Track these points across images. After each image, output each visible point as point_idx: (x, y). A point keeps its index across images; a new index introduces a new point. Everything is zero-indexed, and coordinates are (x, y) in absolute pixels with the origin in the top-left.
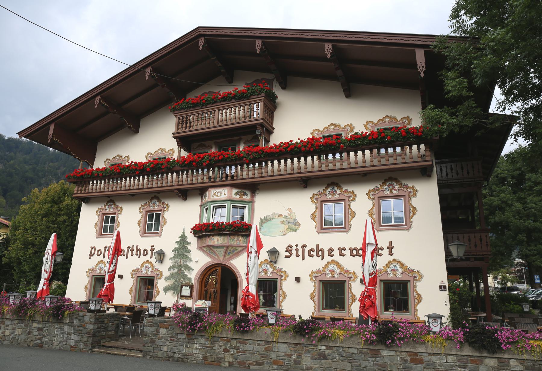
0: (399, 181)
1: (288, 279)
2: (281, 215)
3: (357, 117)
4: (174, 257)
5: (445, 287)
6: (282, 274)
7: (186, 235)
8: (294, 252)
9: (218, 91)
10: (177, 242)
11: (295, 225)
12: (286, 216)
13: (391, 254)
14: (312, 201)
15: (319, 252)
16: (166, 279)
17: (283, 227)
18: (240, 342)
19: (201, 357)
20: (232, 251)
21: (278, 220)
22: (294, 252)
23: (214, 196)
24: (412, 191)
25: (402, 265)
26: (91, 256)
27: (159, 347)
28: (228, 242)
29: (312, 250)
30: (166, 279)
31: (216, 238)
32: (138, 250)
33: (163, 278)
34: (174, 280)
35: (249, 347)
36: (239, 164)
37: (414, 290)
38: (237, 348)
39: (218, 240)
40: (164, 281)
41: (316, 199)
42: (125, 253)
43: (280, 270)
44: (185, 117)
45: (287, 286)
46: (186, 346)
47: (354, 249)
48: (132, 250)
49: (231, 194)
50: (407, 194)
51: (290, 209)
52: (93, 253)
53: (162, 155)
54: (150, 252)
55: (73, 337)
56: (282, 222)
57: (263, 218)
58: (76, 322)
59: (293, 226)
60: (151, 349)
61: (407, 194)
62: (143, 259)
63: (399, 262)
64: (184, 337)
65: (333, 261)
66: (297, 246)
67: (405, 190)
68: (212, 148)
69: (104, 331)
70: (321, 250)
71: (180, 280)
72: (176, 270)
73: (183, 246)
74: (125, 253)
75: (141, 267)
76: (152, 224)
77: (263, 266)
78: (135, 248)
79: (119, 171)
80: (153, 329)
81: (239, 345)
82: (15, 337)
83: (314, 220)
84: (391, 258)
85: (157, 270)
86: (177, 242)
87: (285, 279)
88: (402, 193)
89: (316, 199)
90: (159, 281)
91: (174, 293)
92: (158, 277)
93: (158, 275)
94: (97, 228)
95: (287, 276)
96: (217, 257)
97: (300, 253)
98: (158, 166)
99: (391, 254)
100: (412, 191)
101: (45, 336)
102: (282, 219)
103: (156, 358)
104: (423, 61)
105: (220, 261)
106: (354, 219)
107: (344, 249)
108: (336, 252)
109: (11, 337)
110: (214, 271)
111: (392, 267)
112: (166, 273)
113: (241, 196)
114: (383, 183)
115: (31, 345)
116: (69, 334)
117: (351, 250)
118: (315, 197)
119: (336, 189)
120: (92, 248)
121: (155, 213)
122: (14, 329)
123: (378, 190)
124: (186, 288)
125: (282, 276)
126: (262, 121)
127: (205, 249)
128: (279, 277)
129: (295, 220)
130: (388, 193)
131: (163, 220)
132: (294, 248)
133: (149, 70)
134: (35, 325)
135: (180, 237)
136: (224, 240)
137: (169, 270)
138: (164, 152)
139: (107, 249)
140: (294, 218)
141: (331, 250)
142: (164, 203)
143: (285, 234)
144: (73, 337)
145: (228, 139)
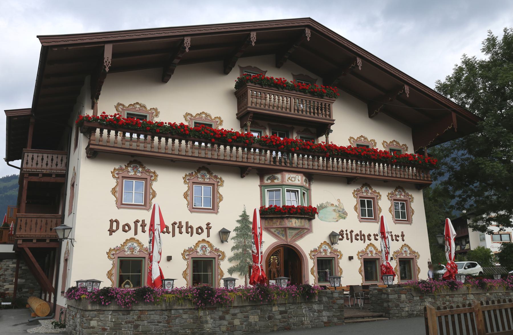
0: (142, 165)
1: (343, 258)
2: (332, 205)
3: (380, 137)
4: (236, 237)
6: (338, 254)
7: (248, 214)
12: (336, 206)
14: (354, 196)
15: (361, 237)
16: (230, 260)
17: (335, 215)
18: (451, 297)
20: (302, 232)
22: (345, 236)
24: (153, 175)
25: (409, 248)
26: (111, 231)
27: (402, 309)
29: (357, 235)
30: (230, 260)
31: (294, 221)
33: (226, 259)
34: (239, 261)
35: (455, 299)
36: (316, 155)
37: (219, 267)
38: (449, 301)
39: (295, 223)
40: (228, 262)
41: (357, 194)
42: (171, 230)
43: (336, 251)
44: (323, 104)
45: (343, 263)
46: (420, 305)
50: (149, 178)
51: (339, 200)
52: (114, 228)
54: (205, 231)
55: (324, 313)
56: (334, 210)
57: (319, 205)
58: (325, 299)
59: (343, 215)
60: (397, 311)
61: (149, 178)
62: (197, 238)
63: (408, 246)
64: (418, 298)
66: (346, 231)
67: (148, 174)
68: (265, 129)
71: (246, 260)
72: (240, 250)
73: (246, 225)
74: (171, 230)
75: (195, 247)
77: (323, 247)
78: (184, 224)
79: (137, 123)
81: (450, 299)
82: (250, 324)
84: (403, 243)
85: (217, 250)
87: (341, 258)
88: (144, 176)
89: (357, 194)
90: (222, 263)
91: (241, 274)
92: (220, 258)
93: (219, 255)
95: (342, 255)
96: (284, 238)
97: (349, 237)
98: (203, 132)
99: (403, 240)
100: (153, 175)
101: (291, 317)
102: (334, 208)
103: (402, 317)
104: (456, 122)
105: (287, 242)
108: (372, 237)
109: (244, 326)
110: (278, 251)
111: (404, 249)
112: (229, 254)
113: (272, 181)
114: (128, 164)
115: (275, 329)
116: (319, 311)
118: (356, 193)
119: (368, 189)
120: (111, 221)
122: (247, 317)
123: (393, 194)
125: (338, 255)
127: (273, 230)
128: (336, 256)
129: (343, 209)
130: (132, 173)
131: (218, 195)
132: (345, 232)
134: (275, 309)
135: (241, 216)
136: (301, 223)
137: (232, 250)
138: (209, 118)
139: (176, 226)
140: (342, 207)
141: (369, 235)
142: (216, 177)
143: (337, 221)
144: (324, 313)
145: (281, 124)
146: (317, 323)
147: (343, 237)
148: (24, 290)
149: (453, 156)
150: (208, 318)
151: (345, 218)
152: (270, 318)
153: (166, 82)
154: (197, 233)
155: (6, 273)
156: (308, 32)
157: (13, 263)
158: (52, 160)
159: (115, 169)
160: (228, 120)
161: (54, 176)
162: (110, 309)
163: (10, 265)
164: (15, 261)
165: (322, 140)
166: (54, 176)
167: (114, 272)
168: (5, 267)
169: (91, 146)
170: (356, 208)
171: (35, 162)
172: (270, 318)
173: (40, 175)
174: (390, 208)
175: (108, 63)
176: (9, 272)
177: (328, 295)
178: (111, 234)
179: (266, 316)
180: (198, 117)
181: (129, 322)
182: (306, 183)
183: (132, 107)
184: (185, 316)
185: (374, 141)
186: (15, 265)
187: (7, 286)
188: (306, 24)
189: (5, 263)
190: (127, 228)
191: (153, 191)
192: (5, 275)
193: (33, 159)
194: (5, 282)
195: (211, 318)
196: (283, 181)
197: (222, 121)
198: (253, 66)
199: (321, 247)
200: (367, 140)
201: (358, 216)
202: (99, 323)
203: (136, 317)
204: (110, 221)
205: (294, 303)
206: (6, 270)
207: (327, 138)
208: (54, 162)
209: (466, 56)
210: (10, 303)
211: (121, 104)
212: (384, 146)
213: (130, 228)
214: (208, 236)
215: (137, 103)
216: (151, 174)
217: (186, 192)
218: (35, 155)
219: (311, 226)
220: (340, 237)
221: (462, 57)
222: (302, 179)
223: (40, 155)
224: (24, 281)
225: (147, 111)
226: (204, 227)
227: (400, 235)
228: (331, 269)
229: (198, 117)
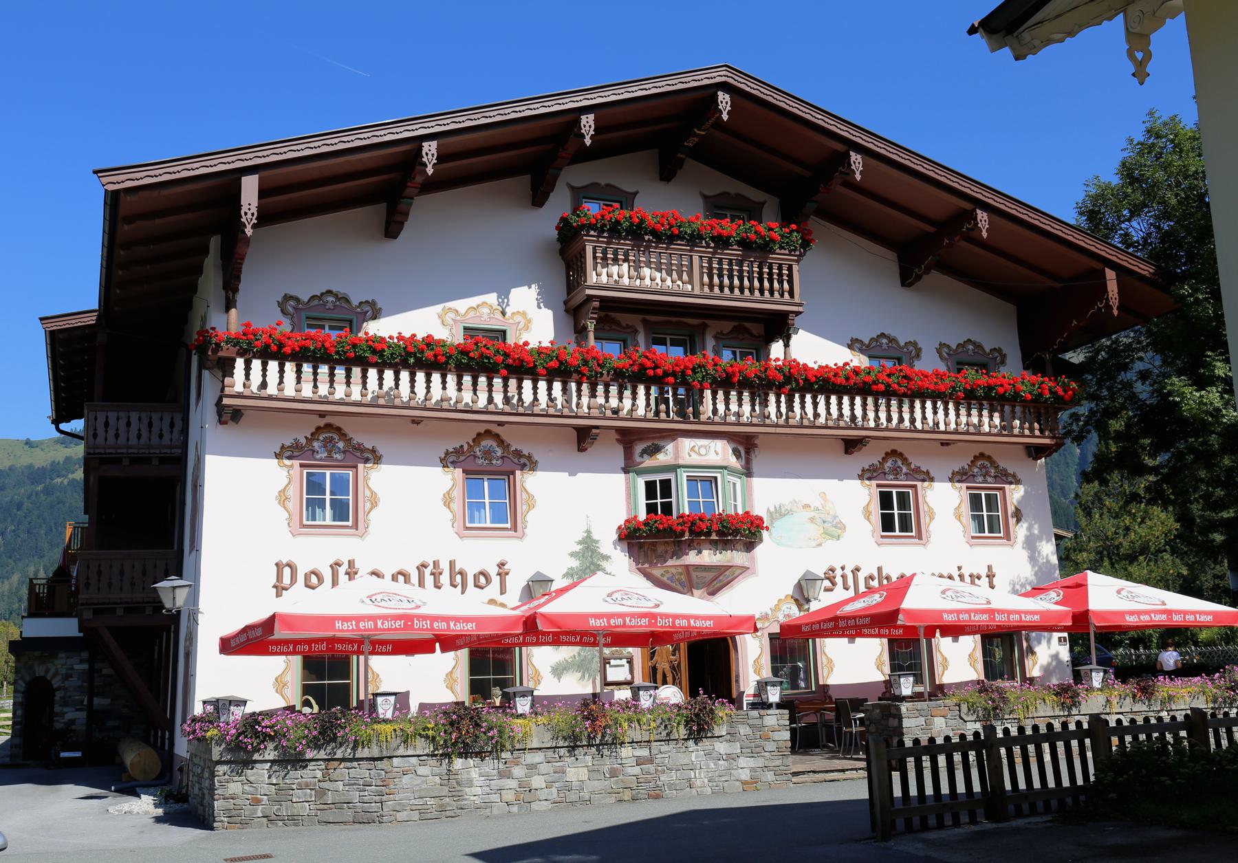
2: (807, 506)
7: (595, 537)
8: (839, 580)
9: (629, 188)
10: (573, 554)
17: (815, 531)
22: (839, 580)
23: (693, 454)
47: (288, 565)
52: (287, 580)
54: (496, 580)
56: (812, 520)
57: (772, 509)
59: (834, 529)
66: (843, 568)
70: (461, 573)
73: (592, 563)
76: (332, 493)
77: (784, 608)
78: (445, 566)
80: (921, 721)
86: (573, 554)
91: (583, 677)
97: (850, 582)
101: (663, 772)
102: (811, 514)
104: (1116, 291)
109: (554, 790)
116: (730, 757)
123: (965, 474)
124: (618, 662)
129: (835, 517)
131: (525, 496)
132: (839, 572)
134: (626, 752)
135: (580, 543)
139: (427, 571)
143: (820, 545)
144: (742, 762)
146: (726, 784)
147: (834, 584)
148: (110, 723)
149: (1139, 366)
150: (474, 774)
151: (838, 538)
152: (613, 773)
153: (396, 237)
154: (476, 586)
155: (67, 684)
156: (724, 99)
157: (82, 662)
158: (150, 425)
159: (283, 447)
160: (533, 321)
161: (155, 462)
162: (267, 757)
163: (76, 667)
164: (85, 655)
165: (777, 350)
166: (155, 462)
167: (288, 678)
168: (64, 671)
169: (226, 401)
170: (867, 513)
171: (111, 432)
172: (613, 773)
173: (126, 462)
174: (282, 492)
175: (249, 216)
176: (74, 682)
177: (750, 722)
178: (278, 595)
179: (606, 768)
180: (472, 314)
181: (307, 785)
182: (738, 456)
183: (316, 302)
184: (422, 770)
185: (915, 344)
186: (85, 666)
187: (71, 714)
188: (718, 80)
189: (63, 661)
190: (314, 579)
191: (372, 492)
192: (65, 689)
193: (107, 424)
194: (66, 704)
195: (481, 775)
196: (677, 456)
197: (529, 321)
198: (603, 182)
199: (780, 609)
200: (897, 343)
201: (873, 532)
202: (246, 787)
203: (319, 774)
204: (277, 564)
205: (668, 740)
206: (67, 677)
207: (787, 345)
208: (155, 430)
209: (1156, 115)
210: (78, 754)
211: (292, 298)
212: (941, 357)
213: (321, 580)
214: (503, 592)
215: (329, 292)
216: (366, 455)
217: (448, 493)
218: (112, 416)
219: (753, 560)
220: (827, 583)
221: (1147, 118)
222: (724, 449)
223: (122, 414)
224: (107, 701)
225: (352, 310)
226: (493, 571)
227: (984, 573)
228: (806, 659)
229: (472, 314)
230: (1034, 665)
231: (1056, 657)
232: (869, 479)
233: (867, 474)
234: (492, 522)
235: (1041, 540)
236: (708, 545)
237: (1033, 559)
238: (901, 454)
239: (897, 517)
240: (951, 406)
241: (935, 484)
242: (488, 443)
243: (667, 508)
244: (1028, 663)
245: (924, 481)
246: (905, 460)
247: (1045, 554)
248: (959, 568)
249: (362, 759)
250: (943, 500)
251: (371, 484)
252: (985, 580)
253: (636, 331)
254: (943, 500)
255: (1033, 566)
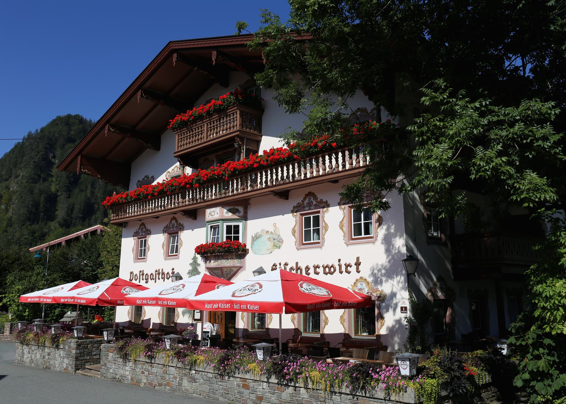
2: (268, 232)
5: (406, 308)
10: (191, 264)
11: (279, 242)
12: (272, 233)
13: (358, 271)
17: (270, 244)
19: (129, 377)
21: (266, 237)
28: (221, 263)
32: (163, 273)
48: (159, 274)
49: (222, 213)
53: (178, 173)
56: (269, 239)
59: (277, 243)
65: (361, 278)
66: (280, 264)
69: (87, 355)
73: (195, 268)
77: (359, 285)
78: (161, 271)
83: (294, 236)
84: (358, 276)
94: (345, 229)
99: (358, 271)
106: (327, 232)
107: (318, 267)
117: (325, 268)
121: (312, 216)
126: (238, 133)
129: (279, 236)
133: (139, 93)
140: (278, 234)
143: (271, 252)
230: (382, 326)
231: (399, 321)
232: (296, 212)
233: (295, 210)
234: (365, 234)
235: (395, 237)
236: (213, 258)
237: (388, 251)
238: (313, 194)
239: (311, 231)
240: (347, 153)
241: (331, 209)
242: (174, 221)
243: (237, 238)
244: (378, 324)
245: (324, 207)
246: (315, 198)
247: (397, 246)
248: (339, 260)
249: (342, 393)
250: (335, 217)
251: (325, 219)
252: (354, 267)
253: (214, 162)
254: (335, 217)
255: (388, 256)
